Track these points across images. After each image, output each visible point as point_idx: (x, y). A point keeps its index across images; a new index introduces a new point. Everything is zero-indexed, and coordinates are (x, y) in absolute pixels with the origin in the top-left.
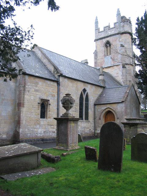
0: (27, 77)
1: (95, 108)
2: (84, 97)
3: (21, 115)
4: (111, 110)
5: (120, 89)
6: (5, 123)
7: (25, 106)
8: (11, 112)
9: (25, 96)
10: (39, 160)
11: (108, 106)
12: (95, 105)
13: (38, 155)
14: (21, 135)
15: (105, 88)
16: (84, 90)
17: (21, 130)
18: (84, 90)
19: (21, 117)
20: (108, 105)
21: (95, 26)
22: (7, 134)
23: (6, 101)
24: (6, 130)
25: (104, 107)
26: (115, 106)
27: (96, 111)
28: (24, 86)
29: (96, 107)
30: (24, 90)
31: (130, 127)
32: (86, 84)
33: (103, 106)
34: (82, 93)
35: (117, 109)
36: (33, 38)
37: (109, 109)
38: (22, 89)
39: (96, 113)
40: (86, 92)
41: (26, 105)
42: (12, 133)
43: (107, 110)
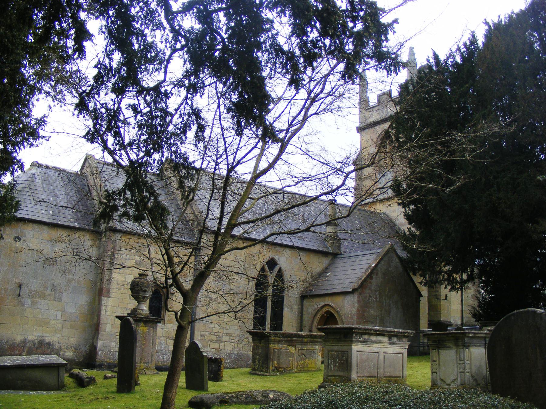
0: (118, 236)
1: (302, 305)
2: (271, 279)
3: (103, 312)
4: (332, 311)
5: (364, 258)
6: (72, 327)
7: (113, 295)
8: (87, 308)
9: (113, 276)
10: (60, 381)
11: (328, 301)
12: (303, 297)
13: (59, 372)
14: (100, 353)
15: (339, 256)
16: (272, 263)
17: (100, 344)
18: (272, 263)
19: (102, 317)
20: (327, 298)
21: (59, 168)
22: (76, 349)
23: (76, 284)
24: (73, 341)
25: (319, 303)
26: (339, 300)
27: (304, 313)
28: (113, 255)
29: (305, 302)
30: (112, 263)
31: (260, 340)
32: (278, 248)
33: (317, 300)
34: (263, 269)
35: (343, 306)
36: (319, 131)
37: (328, 308)
38: (107, 259)
39: (304, 316)
40: (277, 269)
41: (113, 294)
42: (85, 349)
43: (325, 309)
